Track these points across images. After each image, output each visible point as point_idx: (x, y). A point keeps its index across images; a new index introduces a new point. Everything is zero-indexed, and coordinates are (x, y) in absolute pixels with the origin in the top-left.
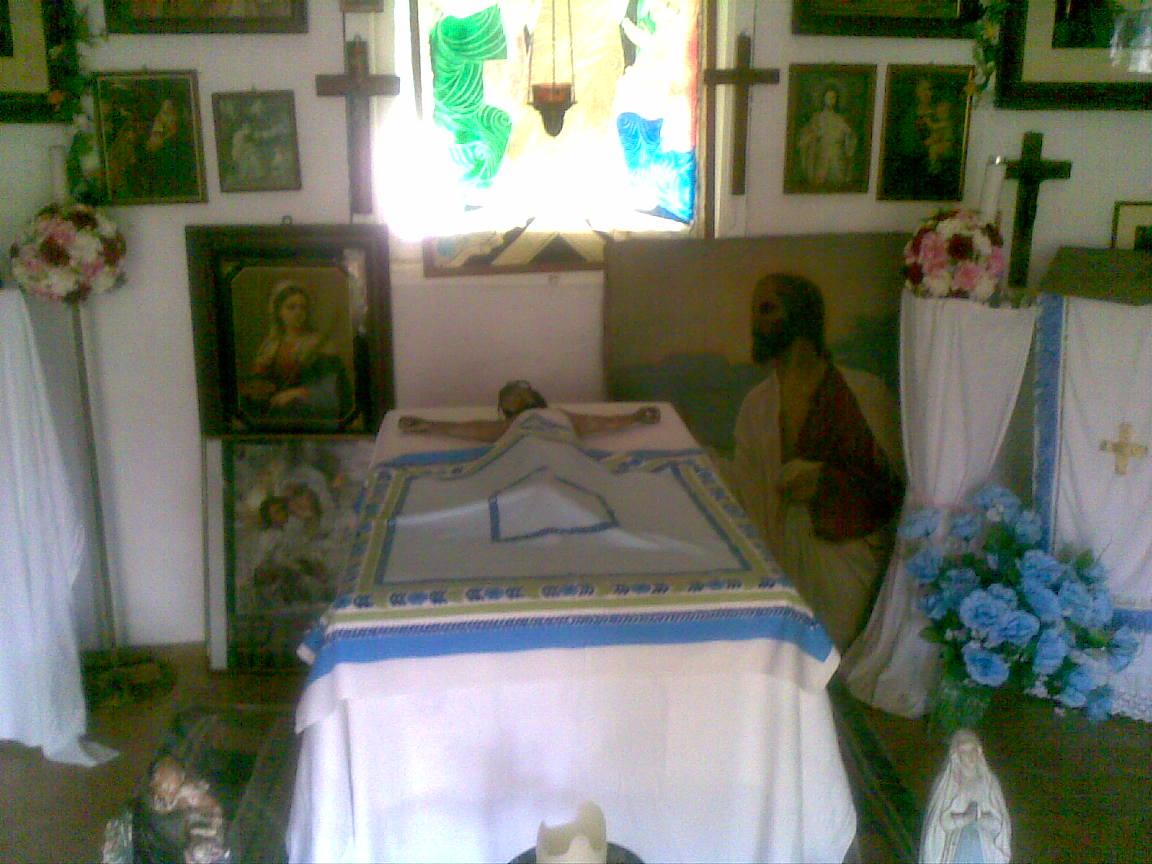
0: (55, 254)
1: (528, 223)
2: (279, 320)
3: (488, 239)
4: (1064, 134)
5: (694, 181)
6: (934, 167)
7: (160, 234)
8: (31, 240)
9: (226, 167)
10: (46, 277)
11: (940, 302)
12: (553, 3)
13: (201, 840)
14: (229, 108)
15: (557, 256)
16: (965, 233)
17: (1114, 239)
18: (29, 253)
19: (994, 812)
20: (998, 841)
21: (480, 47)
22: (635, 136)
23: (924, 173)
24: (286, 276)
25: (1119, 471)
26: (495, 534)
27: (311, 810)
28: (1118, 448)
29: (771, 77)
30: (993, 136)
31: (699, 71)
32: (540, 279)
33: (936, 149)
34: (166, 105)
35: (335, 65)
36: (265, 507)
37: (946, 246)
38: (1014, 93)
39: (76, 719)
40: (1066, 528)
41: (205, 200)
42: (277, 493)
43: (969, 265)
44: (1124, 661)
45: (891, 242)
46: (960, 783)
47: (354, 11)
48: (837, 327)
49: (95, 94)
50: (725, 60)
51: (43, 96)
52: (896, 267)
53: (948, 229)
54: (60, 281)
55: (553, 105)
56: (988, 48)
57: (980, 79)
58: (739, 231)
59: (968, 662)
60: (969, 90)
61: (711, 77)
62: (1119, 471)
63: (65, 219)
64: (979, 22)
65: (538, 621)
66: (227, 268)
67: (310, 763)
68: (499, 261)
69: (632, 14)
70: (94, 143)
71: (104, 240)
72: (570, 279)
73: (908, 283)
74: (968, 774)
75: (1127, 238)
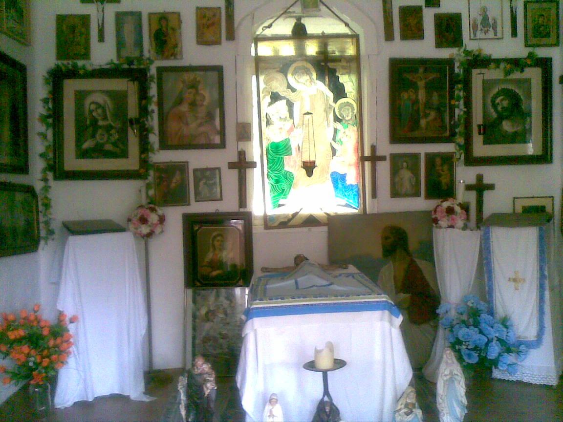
0: (143, 220)
1: (301, 210)
2: (214, 246)
3: (286, 216)
4: (491, 174)
5: (359, 195)
6: (444, 187)
7: (174, 216)
8: (136, 216)
9: (197, 193)
10: (141, 228)
11: (445, 229)
12: (469, 1)
13: (209, 381)
14: (199, 173)
15: (311, 221)
16: (451, 206)
17: (514, 210)
18: (135, 220)
19: (459, 374)
20: (461, 384)
21: (283, 152)
22: (337, 180)
23: (440, 189)
24: (216, 230)
25: (516, 289)
26: (297, 288)
27: (245, 364)
28: (515, 280)
29: (383, 158)
30: (465, 175)
31: (358, 157)
32: (306, 229)
33: (444, 180)
34: (178, 172)
35: (235, 159)
36: (207, 313)
37: (445, 210)
38: (471, 161)
39: (141, 387)
40: (500, 312)
41: (189, 204)
42: (212, 308)
43: (454, 216)
44: (523, 357)
45: (427, 213)
46: (447, 365)
47: (241, 141)
48: (413, 243)
49: (154, 171)
50: (367, 153)
51: (137, 171)
52: (431, 220)
53: (446, 204)
54: (145, 230)
55: (309, 167)
56: (460, 146)
57: (458, 156)
58: (375, 211)
59: (463, 355)
60: (454, 160)
61: (363, 159)
62: (516, 289)
63: (147, 209)
64: (456, 137)
65: (312, 305)
66: (196, 228)
67: (245, 347)
68: (292, 223)
69: (334, 139)
70: (153, 185)
71: (159, 216)
72: (315, 229)
73: (434, 225)
74: (449, 362)
75: (519, 209)
